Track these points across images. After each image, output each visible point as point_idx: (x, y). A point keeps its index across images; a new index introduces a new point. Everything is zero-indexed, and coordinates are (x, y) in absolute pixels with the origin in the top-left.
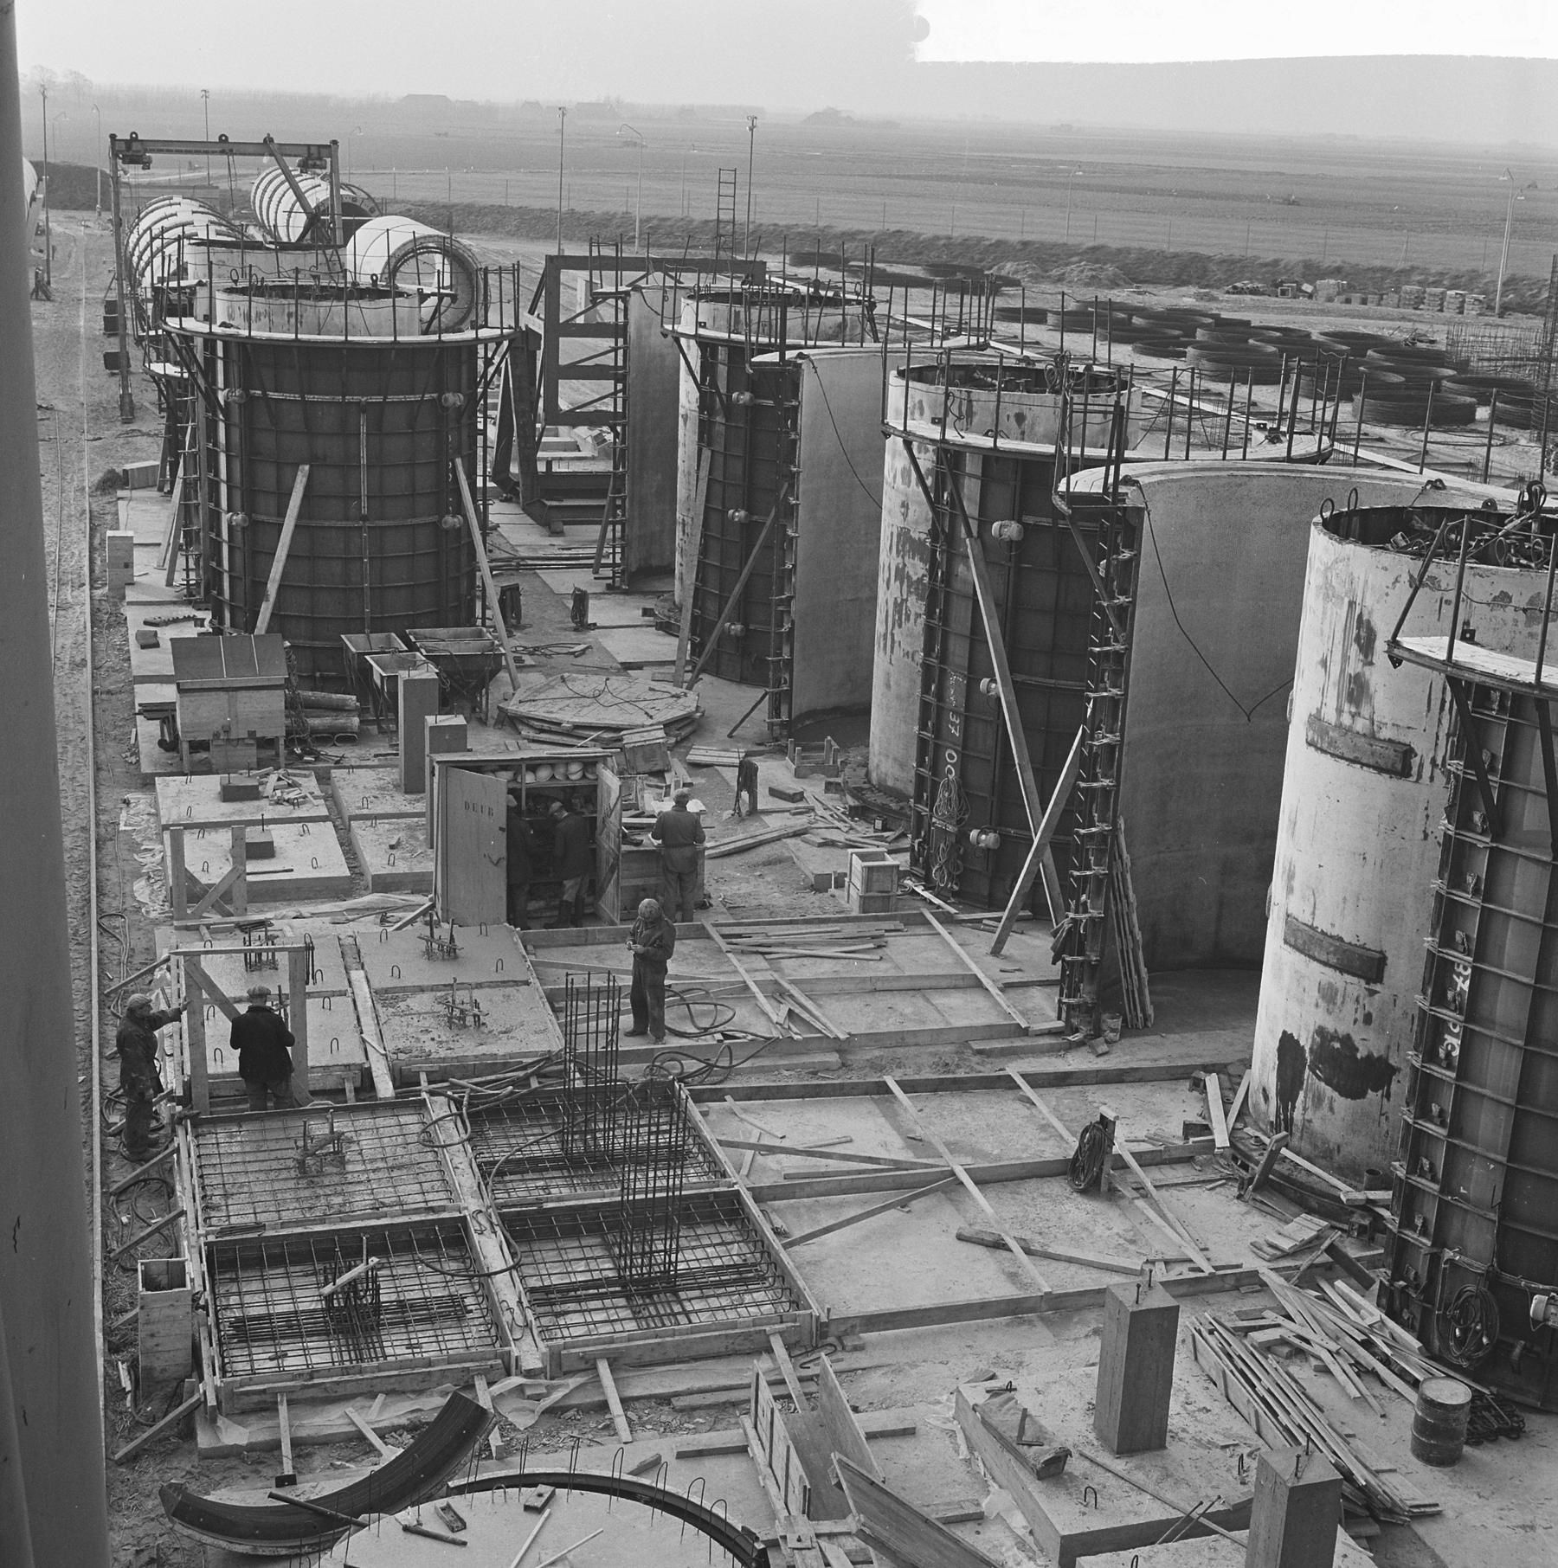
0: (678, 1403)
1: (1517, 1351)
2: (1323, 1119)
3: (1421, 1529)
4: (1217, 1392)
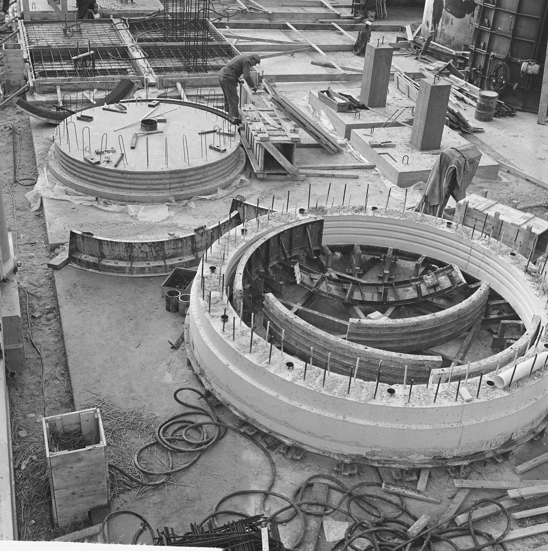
1: (515, 86)
2: (448, 28)
3: (476, 135)
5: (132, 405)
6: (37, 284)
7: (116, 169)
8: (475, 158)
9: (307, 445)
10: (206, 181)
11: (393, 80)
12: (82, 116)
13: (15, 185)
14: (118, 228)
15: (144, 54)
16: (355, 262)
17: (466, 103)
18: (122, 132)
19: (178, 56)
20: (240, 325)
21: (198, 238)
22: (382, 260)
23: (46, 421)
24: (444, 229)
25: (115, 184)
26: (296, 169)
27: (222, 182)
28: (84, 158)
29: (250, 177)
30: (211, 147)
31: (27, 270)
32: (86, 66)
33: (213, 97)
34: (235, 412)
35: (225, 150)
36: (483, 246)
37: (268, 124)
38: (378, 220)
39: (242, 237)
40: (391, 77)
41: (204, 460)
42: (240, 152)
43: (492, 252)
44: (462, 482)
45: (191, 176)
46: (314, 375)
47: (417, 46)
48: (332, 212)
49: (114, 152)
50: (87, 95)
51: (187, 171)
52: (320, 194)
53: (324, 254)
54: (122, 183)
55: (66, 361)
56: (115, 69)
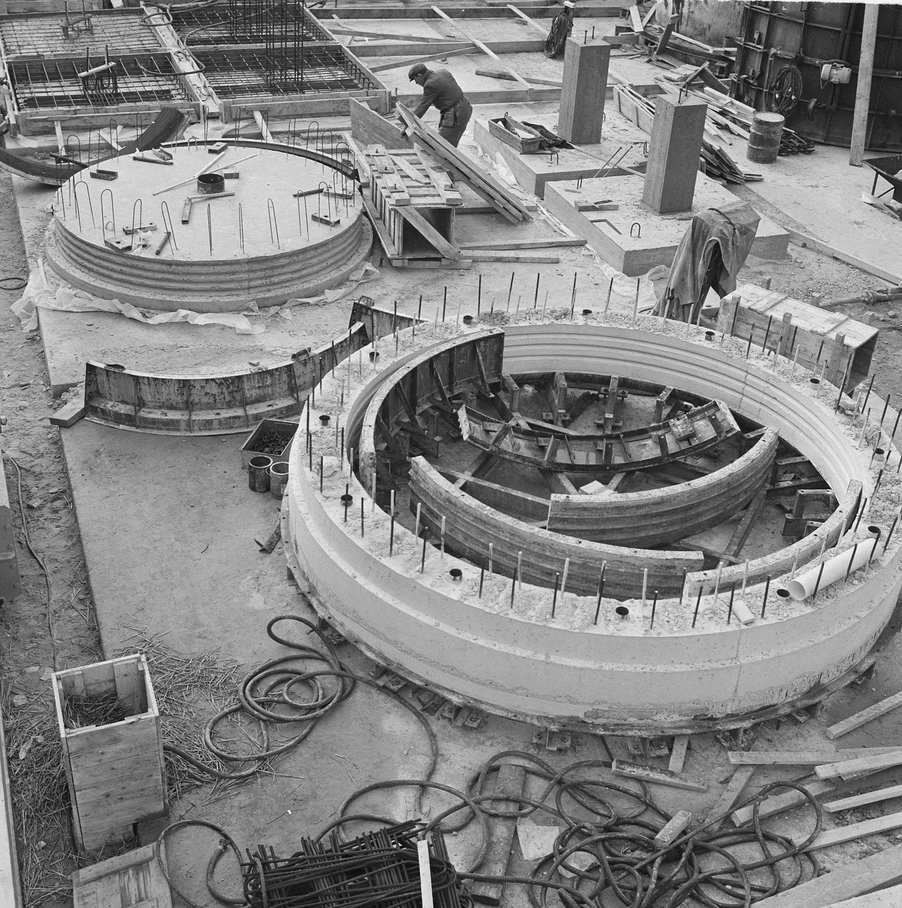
1: (812, 104)
3: (750, 186)
4: (633, 124)
5: (198, 648)
7: (158, 257)
8: (750, 225)
9: (487, 704)
10: (309, 275)
11: (612, 98)
12: (99, 171)
14: (165, 355)
15: (198, 65)
16: (556, 401)
17: (732, 133)
18: (166, 196)
19: (255, 67)
20: (373, 510)
21: (298, 370)
22: (601, 396)
24: (702, 344)
25: (158, 284)
26: (456, 250)
27: (335, 274)
28: (106, 242)
29: (381, 265)
30: (314, 218)
31: (17, 430)
32: (104, 88)
33: (315, 134)
35: (338, 222)
36: (765, 369)
37: (408, 177)
38: (594, 332)
39: (372, 366)
40: (608, 94)
41: (321, 733)
42: (363, 225)
43: (781, 378)
44: (742, 755)
45: (283, 266)
46: (496, 588)
47: (649, 40)
48: (517, 321)
49: (154, 229)
50: (105, 135)
53: (506, 390)
54: (169, 280)
55: (87, 578)
56: (151, 92)
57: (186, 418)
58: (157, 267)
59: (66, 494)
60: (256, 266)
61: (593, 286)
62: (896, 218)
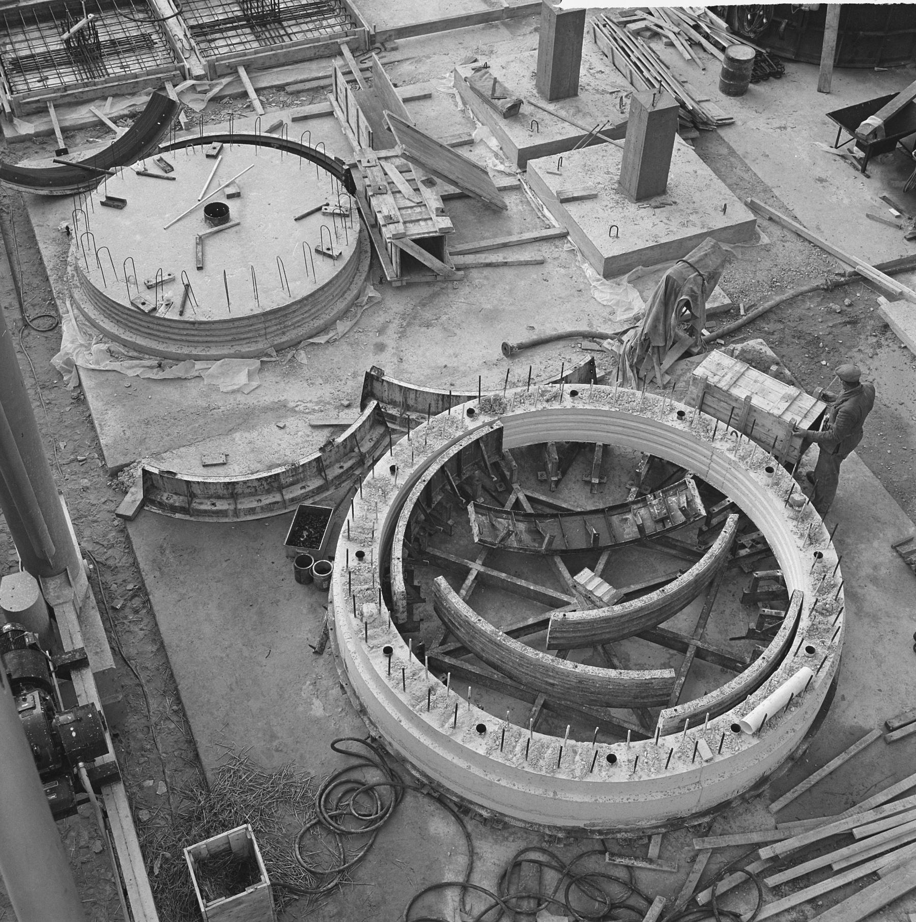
0: (289, 89)
3: (722, 132)
4: (608, 61)
5: (277, 761)
6: (105, 543)
7: (182, 318)
9: (509, 817)
13: (26, 332)
20: (410, 660)
23: (189, 852)
27: (341, 305)
30: (317, 251)
31: (86, 517)
34: (414, 772)
41: (383, 840)
44: (703, 841)
45: (294, 312)
46: (513, 739)
51: (288, 307)
52: (489, 306)
55: (176, 689)
57: (232, 507)
58: (181, 326)
59: (141, 591)
60: (270, 317)
61: (576, 293)
62: (857, 170)
